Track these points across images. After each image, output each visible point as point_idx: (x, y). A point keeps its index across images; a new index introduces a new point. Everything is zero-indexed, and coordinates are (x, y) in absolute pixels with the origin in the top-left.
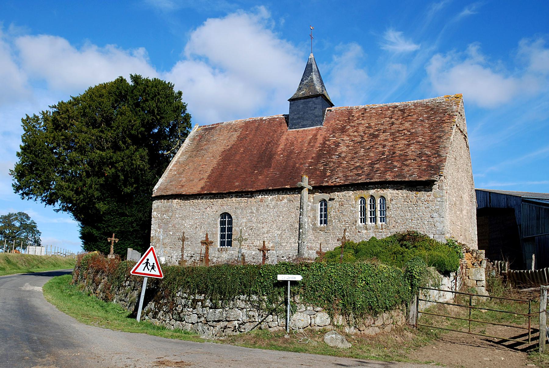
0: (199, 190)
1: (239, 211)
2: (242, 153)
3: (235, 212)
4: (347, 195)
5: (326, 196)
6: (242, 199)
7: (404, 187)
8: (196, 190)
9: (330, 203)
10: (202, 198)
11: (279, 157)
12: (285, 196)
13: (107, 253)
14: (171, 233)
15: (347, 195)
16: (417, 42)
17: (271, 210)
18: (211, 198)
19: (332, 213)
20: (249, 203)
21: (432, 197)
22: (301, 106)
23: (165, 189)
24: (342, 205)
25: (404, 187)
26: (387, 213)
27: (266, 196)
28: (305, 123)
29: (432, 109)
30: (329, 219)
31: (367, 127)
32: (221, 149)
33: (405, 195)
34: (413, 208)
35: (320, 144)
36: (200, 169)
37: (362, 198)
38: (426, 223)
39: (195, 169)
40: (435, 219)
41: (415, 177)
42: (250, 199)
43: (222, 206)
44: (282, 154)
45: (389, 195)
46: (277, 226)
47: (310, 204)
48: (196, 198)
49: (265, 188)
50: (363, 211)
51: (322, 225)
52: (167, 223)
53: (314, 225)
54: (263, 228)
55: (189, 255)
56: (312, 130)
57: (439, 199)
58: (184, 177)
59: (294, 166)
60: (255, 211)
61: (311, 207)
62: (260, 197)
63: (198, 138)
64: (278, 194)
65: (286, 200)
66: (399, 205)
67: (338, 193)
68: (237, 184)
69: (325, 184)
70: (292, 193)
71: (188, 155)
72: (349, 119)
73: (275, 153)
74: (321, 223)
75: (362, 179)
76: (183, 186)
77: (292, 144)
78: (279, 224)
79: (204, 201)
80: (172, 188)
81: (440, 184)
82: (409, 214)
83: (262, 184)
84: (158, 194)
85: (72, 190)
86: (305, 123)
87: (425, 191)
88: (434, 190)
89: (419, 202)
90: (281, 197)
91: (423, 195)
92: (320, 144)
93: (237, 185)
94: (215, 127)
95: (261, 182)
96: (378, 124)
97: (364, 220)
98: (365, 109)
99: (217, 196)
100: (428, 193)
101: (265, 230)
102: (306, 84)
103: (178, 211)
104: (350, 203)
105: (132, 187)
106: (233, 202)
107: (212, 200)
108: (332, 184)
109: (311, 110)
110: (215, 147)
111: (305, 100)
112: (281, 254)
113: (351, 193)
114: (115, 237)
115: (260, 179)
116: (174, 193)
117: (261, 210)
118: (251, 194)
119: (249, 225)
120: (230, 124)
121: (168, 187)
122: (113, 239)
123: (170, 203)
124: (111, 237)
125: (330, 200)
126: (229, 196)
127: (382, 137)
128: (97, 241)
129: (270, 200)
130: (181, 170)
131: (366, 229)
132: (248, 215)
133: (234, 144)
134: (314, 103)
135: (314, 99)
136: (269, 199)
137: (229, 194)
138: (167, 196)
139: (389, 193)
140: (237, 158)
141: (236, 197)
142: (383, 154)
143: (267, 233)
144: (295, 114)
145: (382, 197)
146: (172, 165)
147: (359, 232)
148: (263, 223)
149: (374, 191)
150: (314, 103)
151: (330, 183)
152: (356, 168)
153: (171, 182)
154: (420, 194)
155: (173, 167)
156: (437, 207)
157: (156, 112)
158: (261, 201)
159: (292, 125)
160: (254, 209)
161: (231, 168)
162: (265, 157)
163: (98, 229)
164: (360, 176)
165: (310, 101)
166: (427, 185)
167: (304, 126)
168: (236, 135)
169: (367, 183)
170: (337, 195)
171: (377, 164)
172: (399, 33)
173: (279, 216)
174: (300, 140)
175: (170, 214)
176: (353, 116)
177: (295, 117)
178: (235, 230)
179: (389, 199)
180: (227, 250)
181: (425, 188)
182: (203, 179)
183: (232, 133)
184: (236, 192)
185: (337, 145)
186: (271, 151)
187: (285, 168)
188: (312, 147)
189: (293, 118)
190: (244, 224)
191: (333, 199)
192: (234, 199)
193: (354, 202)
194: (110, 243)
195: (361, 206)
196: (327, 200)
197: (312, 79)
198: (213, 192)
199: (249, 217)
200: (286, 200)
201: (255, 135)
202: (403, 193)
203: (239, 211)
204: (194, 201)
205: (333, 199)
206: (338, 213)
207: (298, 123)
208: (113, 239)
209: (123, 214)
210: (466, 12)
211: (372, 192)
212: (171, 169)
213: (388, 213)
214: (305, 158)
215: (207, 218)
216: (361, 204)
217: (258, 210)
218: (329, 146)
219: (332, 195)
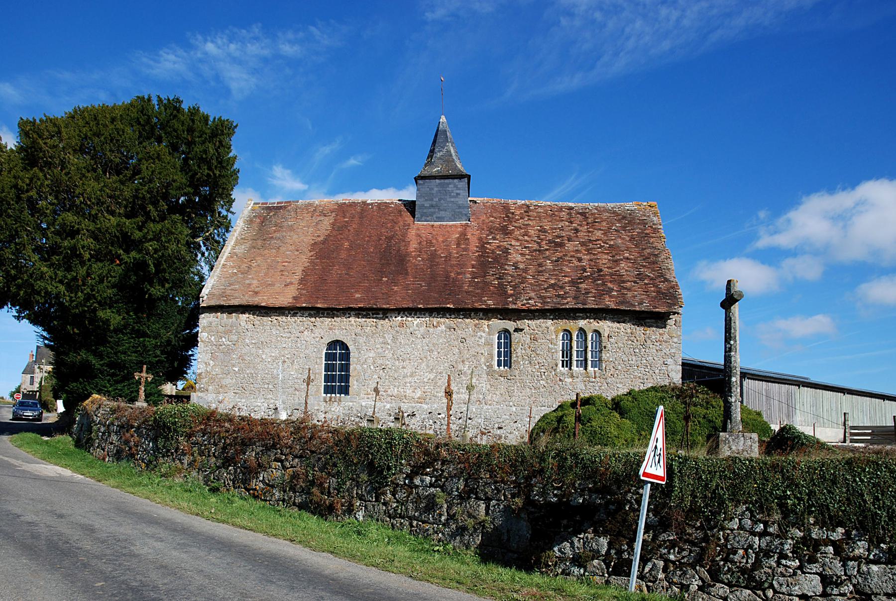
0: (291, 300)
1: (361, 340)
2: (348, 250)
3: (355, 341)
4: (543, 325)
5: (510, 325)
6: (368, 320)
7: (627, 319)
8: (285, 300)
9: (515, 336)
10: (294, 315)
11: (417, 261)
12: (442, 320)
13: (133, 400)
14: (237, 369)
15: (543, 325)
16: (308, 182)
17: (418, 341)
18: (310, 316)
19: (518, 352)
20: (380, 327)
21: (666, 337)
22: (436, 189)
23: (223, 295)
24: (535, 340)
25: (627, 319)
26: (603, 355)
27: (409, 319)
28: (442, 214)
29: (624, 218)
30: (514, 358)
31: (539, 231)
32: (309, 240)
33: (629, 331)
34: (640, 350)
35: (477, 247)
36: (280, 268)
37: (565, 330)
38: (657, 371)
39: (270, 267)
40: (670, 367)
41: (646, 306)
42: (382, 322)
43: (331, 329)
44: (419, 256)
45: (607, 329)
46: (428, 366)
47: (484, 335)
48: (283, 314)
49: (411, 306)
50: (567, 352)
51: (502, 368)
52: (228, 352)
53: (490, 366)
54: (404, 368)
55: (271, 406)
56: (455, 226)
57: (675, 340)
58: (253, 279)
59: (448, 277)
60: (389, 341)
61: (486, 339)
62: (399, 318)
63: (258, 220)
64: (430, 316)
65: (443, 327)
66: (620, 345)
67: (530, 322)
68: (358, 295)
69: (511, 306)
70: (453, 316)
71: (248, 245)
72: (508, 217)
73: (408, 254)
74: (499, 365)
75: (570, 303)
76: (256, 293)
77: (430, 243)
78: (431, 363)
79: (298, 319)
80: (237, 295)
81: (678, 319)
82: (634, 358)
83: (403, 299)
84: (213, 303)
85: (61, 282)
86: (442, 214)
87: (657, 327)
88: (668, 327)
89: (649, 342)
90: (435, 321)
91: (654, 333)
92: (477, 247)
93: (358, 298)
94: (285, 207)
95: (399, 296)
96: (556, 229)
97: (568, 364)
98: (528, 207)
99: (323, 314)
100: (661, 331)
101: (408, 371)
102: (440, 158)
103: (249, 334)
104: (548, 337)
105: (163, 286)
106: (352, 325)
107: (313, 319)
108: (524, 307)
109: (451, 197)
110: (295, 236)
111: (442, 181)
112: (436, 409)
113: (550, 322)
114: (147, 372)
115: (396, 292)
116: (244, 303)
117: (401, 339)
118: (383, 313)
119: (380, 362)
120: (310, 205)
121: (228, 292)
122: (144, 374)
123: (234, 319)
124: (141, 372)
125: (516, 330)
126: (344, 314)
127: (570, 246)
128: (96, 377)
129: (417, 326)
130: (244, 266)
131: (572, 376)
132: (378, 346)
133: (329, 235)
134: (456, 186)
135: (456, 181)
136: (415, 323)
137: (346, 311)
138: (230, 306)
139: (606, 326)
140: (343, 255)
141: (357, 316)
142: (585, 270)
143: (411, 376)
144: (426, 200)
145: (596, 331)
146: (225, 258)
147: (560, 380)
148: (403, 361)
149: (586, 321)
150: (456, 186)
151: (519, 305)
152: (552, 286)
153: (231, 285)
154: (649, 331)
155: (226, 260)
156: (673, 351)
157: (214, 162)
158: (402, 325)
159: (422, 216)
160: (389, 338)
161: (337, 271)
162: (392, 260)
163: (100, 356)
164: (566, 299)
165: (450, 183)
166: (658, 319)
167: (440, 219)
168: (326, 224)
169: (576, 309)
170: (525, 323)
171: (581, 283)
172: (289, 171)
173: (431, 351)
174: (441, 239)
175: (235, 338)
176: (513, 213)
177: (427, 204)
178: (355, 369)
179: (606, 335)
180: (340, 400)
181: (656, 322)
182: (291, 283)
183: (319, 218)
184: (361, 309)
185: (506, 251)
186: (399, 250)
187: (433, 277)
188: (465, 250)
189: (423, 205)
190: (370, 361)
191: (522, 330)
192: (352, 319)
193: (554, 337)
194: (139, 383)
195: (563, 344)
196: (512, 331)
197: (449, 151)
198: (319, 306)
199: (380, 350)
200: (443, 327)
201: (361, 224)
202: (625, 328)
203: (361, 340)
204: (279, 318)
205: (522, 330)
206: (529, 351)
207: (431, 215)
208: (144, 374)
209: (142, 334)
210: (353, 162)
211: (582, 323)
212: (224, 265)
213: (605, 356)
214: (462, 265)
215: (303, 347)
216: (563, 339)
217: (394, 339)
218: (493, 252)
219: (519, 324)
